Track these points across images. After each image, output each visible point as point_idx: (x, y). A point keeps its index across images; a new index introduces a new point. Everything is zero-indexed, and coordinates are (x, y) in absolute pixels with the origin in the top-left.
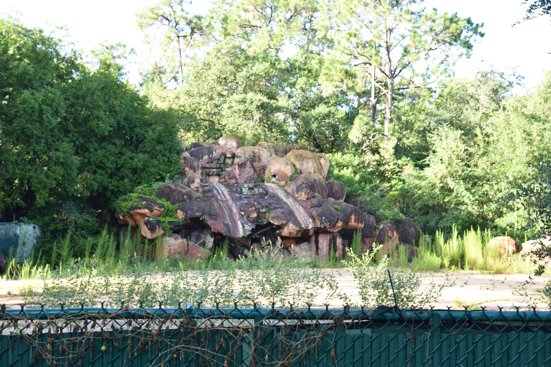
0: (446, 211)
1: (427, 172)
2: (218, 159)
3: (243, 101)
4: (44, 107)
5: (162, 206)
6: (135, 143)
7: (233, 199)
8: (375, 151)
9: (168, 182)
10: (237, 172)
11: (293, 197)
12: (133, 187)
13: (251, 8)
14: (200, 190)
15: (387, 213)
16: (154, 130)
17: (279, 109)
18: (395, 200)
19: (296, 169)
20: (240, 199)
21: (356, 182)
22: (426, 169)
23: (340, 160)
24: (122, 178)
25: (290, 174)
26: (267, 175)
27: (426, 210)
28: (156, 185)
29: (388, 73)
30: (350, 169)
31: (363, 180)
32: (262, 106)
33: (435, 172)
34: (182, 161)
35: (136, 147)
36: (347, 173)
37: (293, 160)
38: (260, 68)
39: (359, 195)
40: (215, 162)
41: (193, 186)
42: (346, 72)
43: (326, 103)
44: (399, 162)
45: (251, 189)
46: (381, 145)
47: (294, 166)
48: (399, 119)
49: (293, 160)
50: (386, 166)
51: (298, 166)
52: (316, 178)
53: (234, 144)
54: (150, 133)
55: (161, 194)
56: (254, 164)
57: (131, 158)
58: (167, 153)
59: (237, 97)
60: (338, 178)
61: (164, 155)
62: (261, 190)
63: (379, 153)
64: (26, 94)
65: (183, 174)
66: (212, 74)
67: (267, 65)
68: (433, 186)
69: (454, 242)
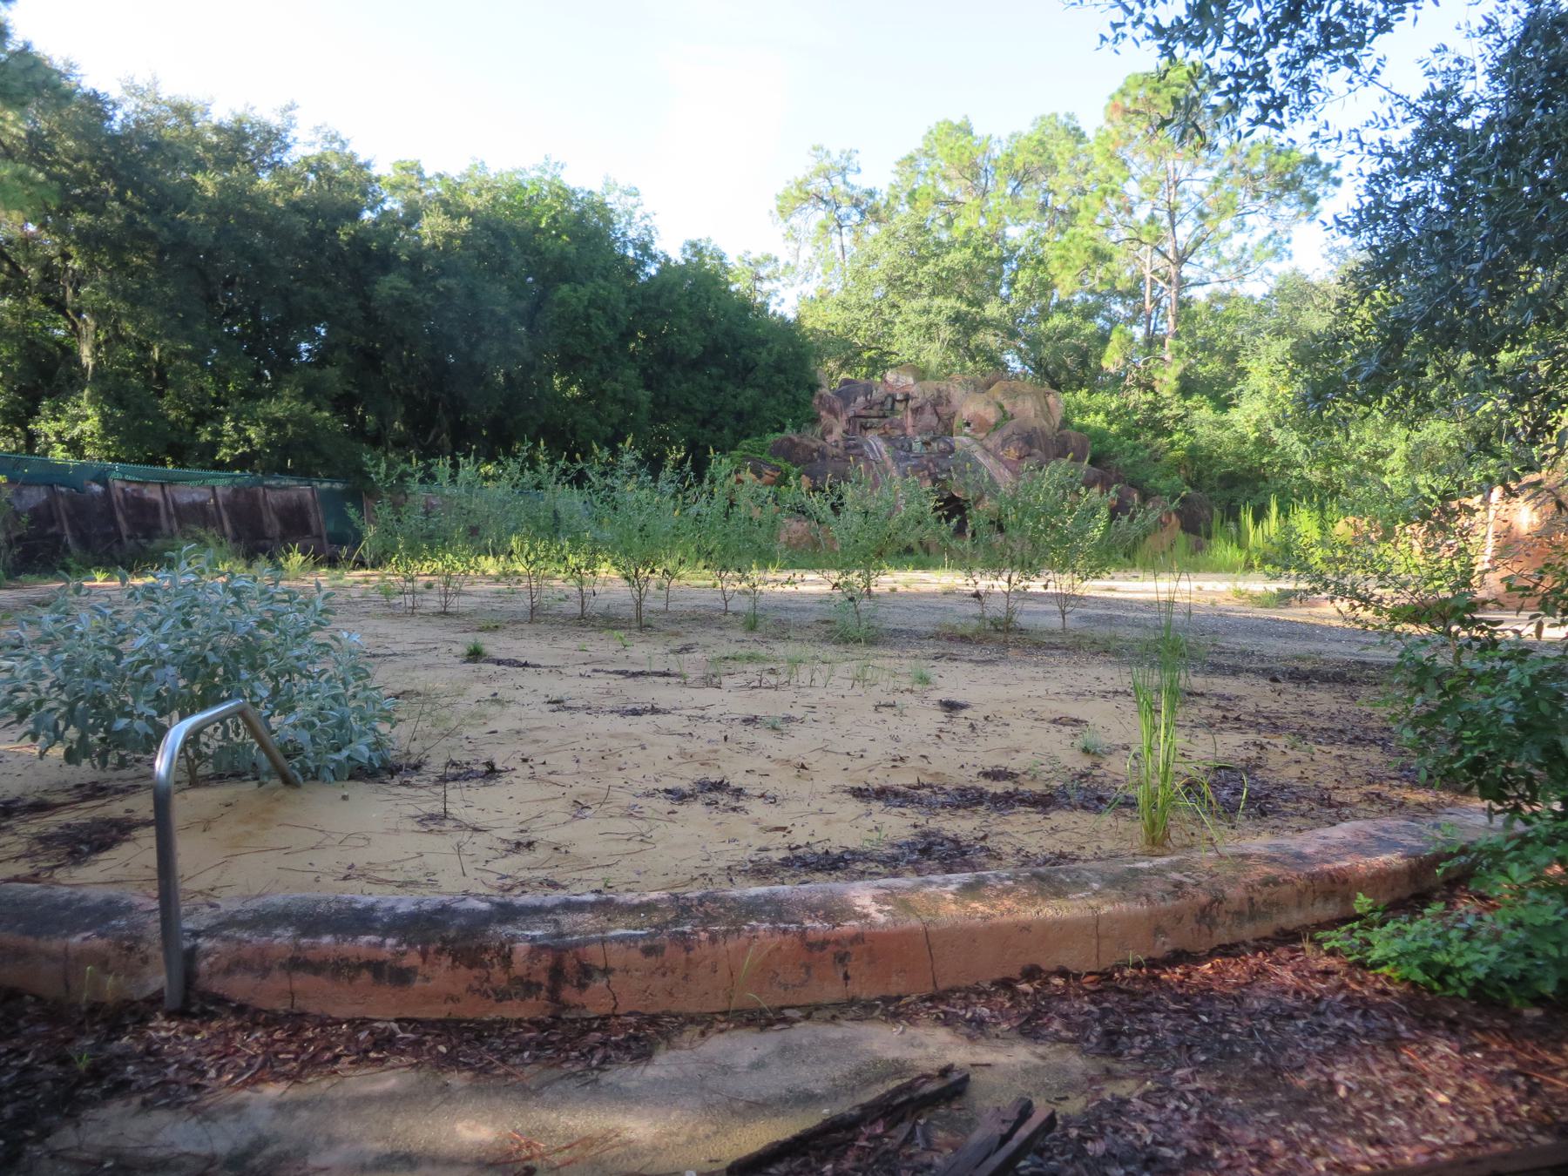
0: (1265, 479)
1: (1234, 415)
2: (882, 403)
3: (927, 311)
4: (592, 311)
5: (777, 469)
6: (743, 372)
7: (894, 459)
8: (1148, 387)
9: (790, 433)
10: (910, 421)
11: (996, 456)
12: (737, 442)
13: (953, 173)
14: (841, 444)
15: (1162, 484)
16: (770, 352)
17: (986, 323)
18: (1178, 465)
19: (1005, 413)
20: (907, 459)
21: (1112, 436)
22: (1232, 410)
23: (1085, 402)
24: (720, 428)
25: (993, 421)
26: (957, 422)
27: (1231, 481)
28: (771, 438)
29: (1171, 256)
30: (1101, 416)
31: (1127, 433)
32: (956, 318)
33: (1248, 415)
34: (816, 401)
35: (743, 379)
36: (1096, 421)
37: (999, 397)
38: (955, 258)
39: (1115, 457)
40: (876, 408)
41: (830, 439)
42: (1096, 251)
43: (1065, 311)
44: (1188, 403)
45: (926, 444)
46: (1157, 375)
47: (1001, 407)
48: (1191, 334)
49: (999, 397)
50: (1166, 411)
51: (1007, 408)
52: (1036, 424)
53: (911, 380)
54: (764, 354)
55: (777, 451)
56: (939, 409)
57: (735, 397)
58: (791, 387)
59: (918, 304)
60: (1081, 429)
61: (787, 392)
62: (942, 445)
63: (1153, 389)
64: (565, 289)
65: (815, 420)
66: (877, 272)
67: (968, 252)
68: (1242, 440)
69: (1272, 524)
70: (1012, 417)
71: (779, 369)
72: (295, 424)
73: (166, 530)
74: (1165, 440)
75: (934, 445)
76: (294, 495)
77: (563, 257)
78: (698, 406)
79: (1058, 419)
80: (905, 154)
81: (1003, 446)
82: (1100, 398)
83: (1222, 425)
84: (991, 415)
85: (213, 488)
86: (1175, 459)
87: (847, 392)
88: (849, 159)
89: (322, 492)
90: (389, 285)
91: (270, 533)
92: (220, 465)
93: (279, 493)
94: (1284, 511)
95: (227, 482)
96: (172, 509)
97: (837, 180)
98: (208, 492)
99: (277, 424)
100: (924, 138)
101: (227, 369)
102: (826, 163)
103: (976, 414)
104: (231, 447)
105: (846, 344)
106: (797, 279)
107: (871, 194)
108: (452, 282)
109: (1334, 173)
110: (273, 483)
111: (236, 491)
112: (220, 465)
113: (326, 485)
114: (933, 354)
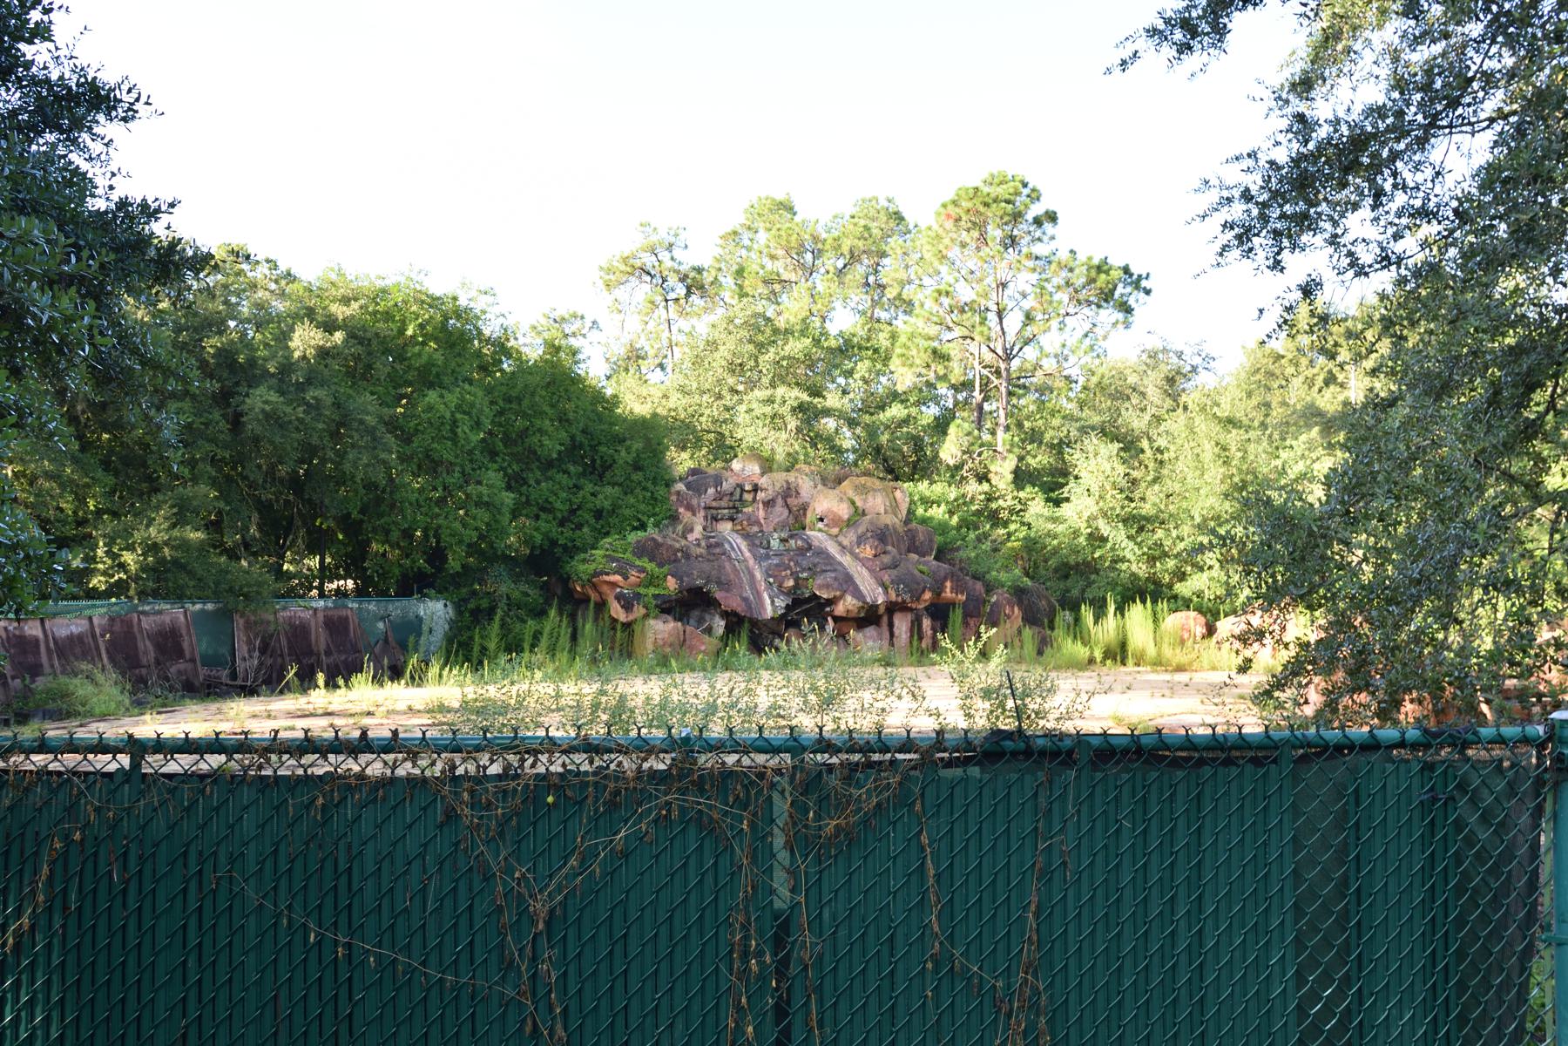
0: (1097, 572)
1: (1066, 510)
4: (458, 416)
5: (643, 570)
8: (983, 477)
9: (651, 531)
10: (761, 514)
11: (852, 553)
13: (781, 252)
14: (703, 544)
15: (1003, 576)
16: (628, 450)
17: (827, 412)
18: (1015, 556)
20: (768, 557)
23: (928, 493)
24: (579, 527)
26: (810, 518)
28: (633, 537)
31: (965, 524)
35: (601, 476)
36: (938, 513)
37: (851, 493)
38: (796, 347)
39: (958, 549)
40: (726, 498)
41: (691, 537)
43: (902, 402)
44: (1022, 494)
45: (783, 541)
46: (992, 468)
47: (853, 503)
48: (1020, 425)
49: (851, 493)
50: (1001, 502)
51: (859, 504)
53: (757, 469)
54: (623, 453)
55: (641, 550)
58: (649, 484)
63: (988, 481)
64: (432, 396)
65: (675, 518)
67: (808, 341)
69: (1111, 622)
70: (864, 514)
71: (637, 467)
72: (172, 548)
73: (47, 669)
74: (1002, 531)
75: (792, 542)
76: (167, 619)
77: (431, 364)
78: (558, 505)
79: (904, 512)
80: (729, 230)
81: (859, 544)
82: (938, 488)
83: (1054, 520)
84: (844, 511)
85: (90, 619)
86: (1013, 549)
87: (697, 480)
88: (676, 235)
89: (195, 614)
90: (260, 399)
91: (144, 661)
92: (93, 594)
93: (152, 618)
94: (1120, 610)
95: (103, 610)
96: (52, 645)
97: (664, 256)
98: (85, 622)
99: (153, 548)
100: (746, 211)
101: (87, 486)
102: (654, 239)
103: (830, 511)
104: (105, 573)
105: (687, 427)
106: (638, 358)
107: (699, 270)
108: (320, 393)
109: (1144, 283)
110: (147, 608)
111: (112, 619)
112: (93, 594)
113: (198, 606)
114: (781, 443)
